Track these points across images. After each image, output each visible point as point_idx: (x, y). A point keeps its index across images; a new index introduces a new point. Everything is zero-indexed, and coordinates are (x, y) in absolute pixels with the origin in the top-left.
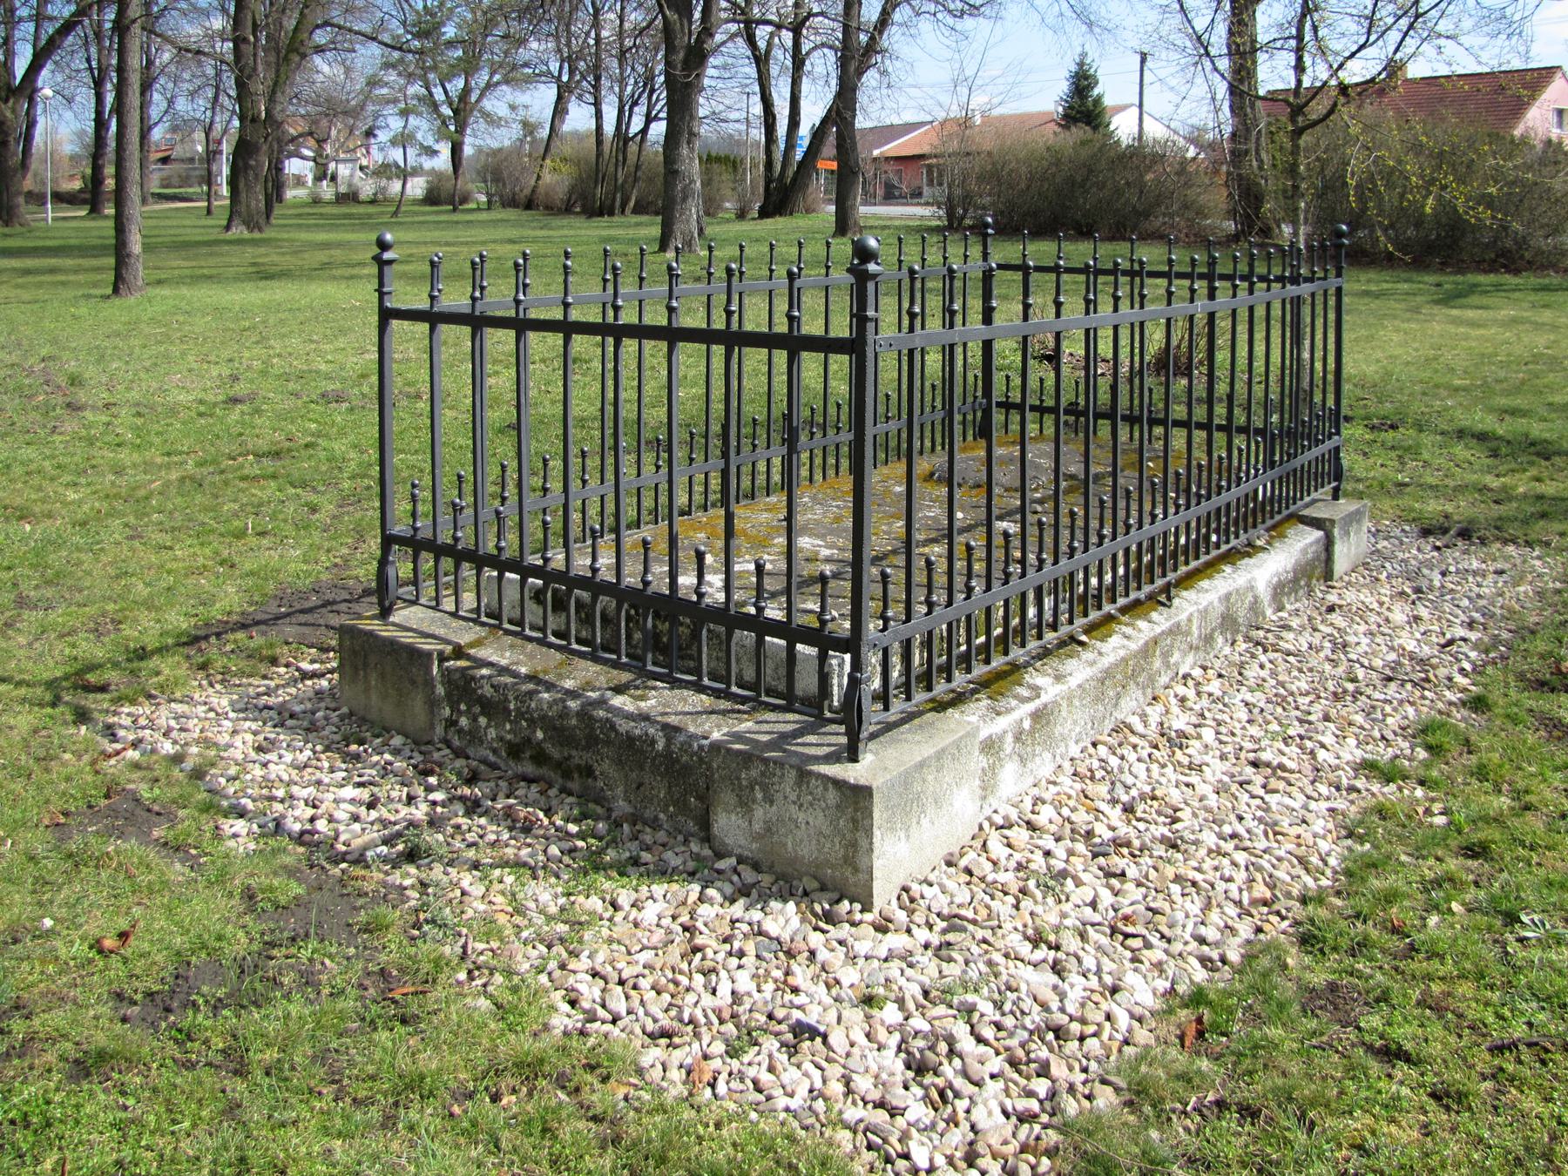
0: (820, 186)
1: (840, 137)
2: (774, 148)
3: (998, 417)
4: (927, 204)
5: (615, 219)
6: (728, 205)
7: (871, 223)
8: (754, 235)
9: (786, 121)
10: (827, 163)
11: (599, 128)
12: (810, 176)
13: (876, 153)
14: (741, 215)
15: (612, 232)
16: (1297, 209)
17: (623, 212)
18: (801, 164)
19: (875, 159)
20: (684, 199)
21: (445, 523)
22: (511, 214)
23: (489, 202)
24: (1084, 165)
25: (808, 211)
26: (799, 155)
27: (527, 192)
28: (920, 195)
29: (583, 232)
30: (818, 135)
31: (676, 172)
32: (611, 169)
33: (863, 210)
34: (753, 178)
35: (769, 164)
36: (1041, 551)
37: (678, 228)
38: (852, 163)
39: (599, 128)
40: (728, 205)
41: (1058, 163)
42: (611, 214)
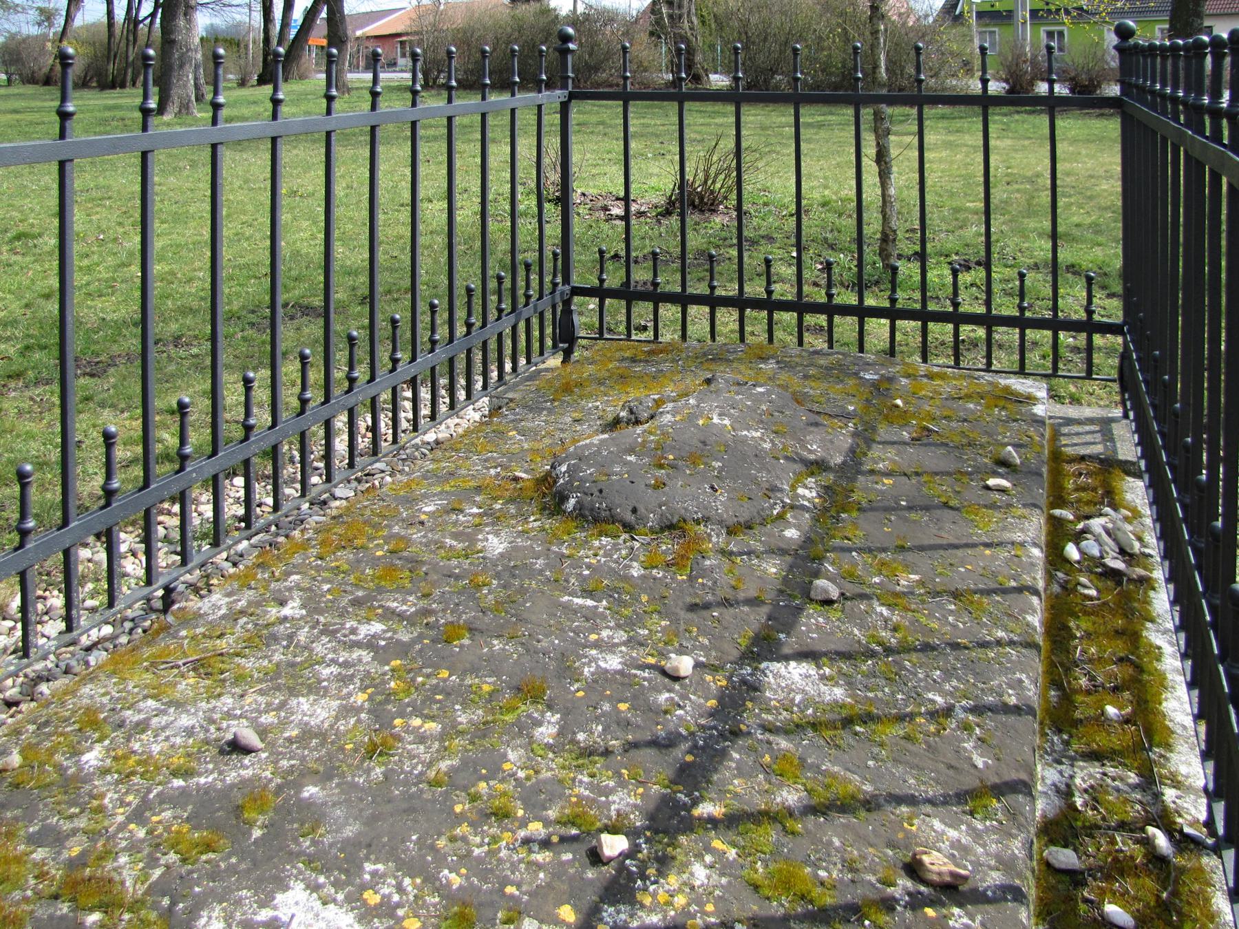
0: (311, 58)
1: (330, 20)
2: (271, 26)
3: (586, 311)
4: (402, 71)
5: (127, 90)
6: (231, 76)
7: (357, 85)
8: (251, 99)
9: (281, 10)
10: (318, 37)
11: (110, 13)
12: (303, 49)
13: (359, 33)
14: (242, 83)
15: (120, 101)
16: (877, 31)
17: (134, 85)
18: (294, 41)
19: (358, 38)
20: (181, 66)
21: (178, 219)
22: (30, 89)
23: (9, 80)
24: (542, 31)
25: (302, 77)
26: (293, 33)
27: (45, 70)
28: (395, 64)
29: (92, 102)
30: (311, 14)
31: (173, 42)
32: (123, 44)
33: (350, 76)
34: (254, 50)
35: (267, 40)
36: (469, 314)
37: (175, 93)
38: (341, 33)
39: (110, 13)
40: (231, 76)
41: (520, 29)
42: (123, 86)
